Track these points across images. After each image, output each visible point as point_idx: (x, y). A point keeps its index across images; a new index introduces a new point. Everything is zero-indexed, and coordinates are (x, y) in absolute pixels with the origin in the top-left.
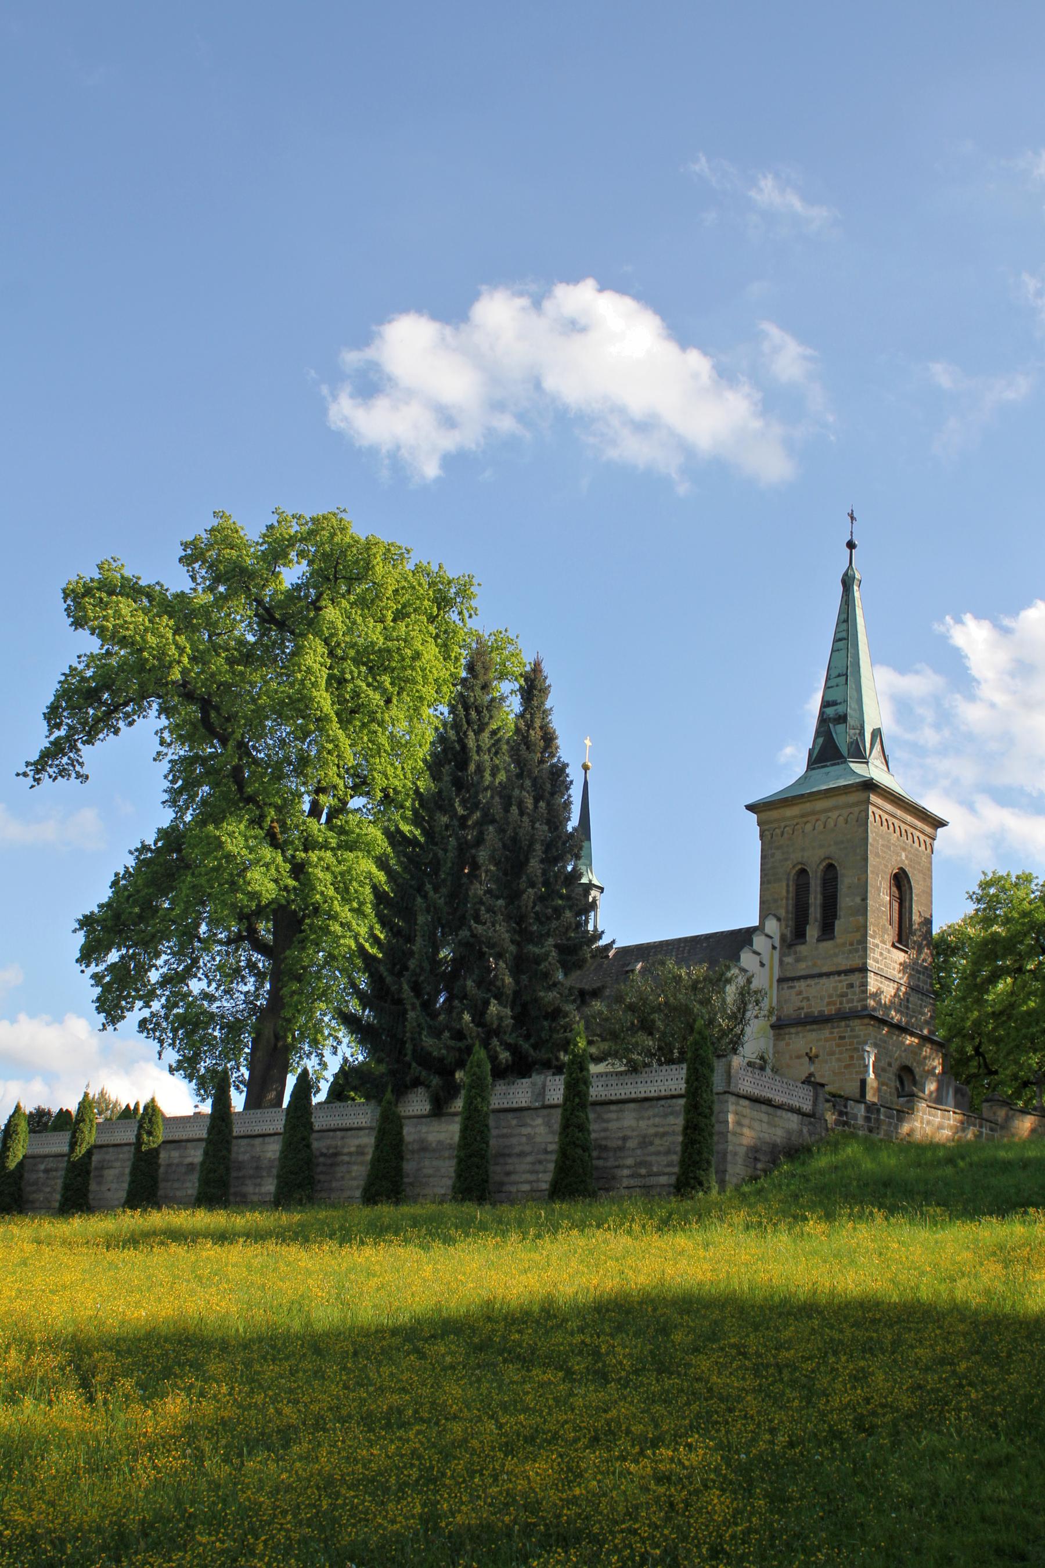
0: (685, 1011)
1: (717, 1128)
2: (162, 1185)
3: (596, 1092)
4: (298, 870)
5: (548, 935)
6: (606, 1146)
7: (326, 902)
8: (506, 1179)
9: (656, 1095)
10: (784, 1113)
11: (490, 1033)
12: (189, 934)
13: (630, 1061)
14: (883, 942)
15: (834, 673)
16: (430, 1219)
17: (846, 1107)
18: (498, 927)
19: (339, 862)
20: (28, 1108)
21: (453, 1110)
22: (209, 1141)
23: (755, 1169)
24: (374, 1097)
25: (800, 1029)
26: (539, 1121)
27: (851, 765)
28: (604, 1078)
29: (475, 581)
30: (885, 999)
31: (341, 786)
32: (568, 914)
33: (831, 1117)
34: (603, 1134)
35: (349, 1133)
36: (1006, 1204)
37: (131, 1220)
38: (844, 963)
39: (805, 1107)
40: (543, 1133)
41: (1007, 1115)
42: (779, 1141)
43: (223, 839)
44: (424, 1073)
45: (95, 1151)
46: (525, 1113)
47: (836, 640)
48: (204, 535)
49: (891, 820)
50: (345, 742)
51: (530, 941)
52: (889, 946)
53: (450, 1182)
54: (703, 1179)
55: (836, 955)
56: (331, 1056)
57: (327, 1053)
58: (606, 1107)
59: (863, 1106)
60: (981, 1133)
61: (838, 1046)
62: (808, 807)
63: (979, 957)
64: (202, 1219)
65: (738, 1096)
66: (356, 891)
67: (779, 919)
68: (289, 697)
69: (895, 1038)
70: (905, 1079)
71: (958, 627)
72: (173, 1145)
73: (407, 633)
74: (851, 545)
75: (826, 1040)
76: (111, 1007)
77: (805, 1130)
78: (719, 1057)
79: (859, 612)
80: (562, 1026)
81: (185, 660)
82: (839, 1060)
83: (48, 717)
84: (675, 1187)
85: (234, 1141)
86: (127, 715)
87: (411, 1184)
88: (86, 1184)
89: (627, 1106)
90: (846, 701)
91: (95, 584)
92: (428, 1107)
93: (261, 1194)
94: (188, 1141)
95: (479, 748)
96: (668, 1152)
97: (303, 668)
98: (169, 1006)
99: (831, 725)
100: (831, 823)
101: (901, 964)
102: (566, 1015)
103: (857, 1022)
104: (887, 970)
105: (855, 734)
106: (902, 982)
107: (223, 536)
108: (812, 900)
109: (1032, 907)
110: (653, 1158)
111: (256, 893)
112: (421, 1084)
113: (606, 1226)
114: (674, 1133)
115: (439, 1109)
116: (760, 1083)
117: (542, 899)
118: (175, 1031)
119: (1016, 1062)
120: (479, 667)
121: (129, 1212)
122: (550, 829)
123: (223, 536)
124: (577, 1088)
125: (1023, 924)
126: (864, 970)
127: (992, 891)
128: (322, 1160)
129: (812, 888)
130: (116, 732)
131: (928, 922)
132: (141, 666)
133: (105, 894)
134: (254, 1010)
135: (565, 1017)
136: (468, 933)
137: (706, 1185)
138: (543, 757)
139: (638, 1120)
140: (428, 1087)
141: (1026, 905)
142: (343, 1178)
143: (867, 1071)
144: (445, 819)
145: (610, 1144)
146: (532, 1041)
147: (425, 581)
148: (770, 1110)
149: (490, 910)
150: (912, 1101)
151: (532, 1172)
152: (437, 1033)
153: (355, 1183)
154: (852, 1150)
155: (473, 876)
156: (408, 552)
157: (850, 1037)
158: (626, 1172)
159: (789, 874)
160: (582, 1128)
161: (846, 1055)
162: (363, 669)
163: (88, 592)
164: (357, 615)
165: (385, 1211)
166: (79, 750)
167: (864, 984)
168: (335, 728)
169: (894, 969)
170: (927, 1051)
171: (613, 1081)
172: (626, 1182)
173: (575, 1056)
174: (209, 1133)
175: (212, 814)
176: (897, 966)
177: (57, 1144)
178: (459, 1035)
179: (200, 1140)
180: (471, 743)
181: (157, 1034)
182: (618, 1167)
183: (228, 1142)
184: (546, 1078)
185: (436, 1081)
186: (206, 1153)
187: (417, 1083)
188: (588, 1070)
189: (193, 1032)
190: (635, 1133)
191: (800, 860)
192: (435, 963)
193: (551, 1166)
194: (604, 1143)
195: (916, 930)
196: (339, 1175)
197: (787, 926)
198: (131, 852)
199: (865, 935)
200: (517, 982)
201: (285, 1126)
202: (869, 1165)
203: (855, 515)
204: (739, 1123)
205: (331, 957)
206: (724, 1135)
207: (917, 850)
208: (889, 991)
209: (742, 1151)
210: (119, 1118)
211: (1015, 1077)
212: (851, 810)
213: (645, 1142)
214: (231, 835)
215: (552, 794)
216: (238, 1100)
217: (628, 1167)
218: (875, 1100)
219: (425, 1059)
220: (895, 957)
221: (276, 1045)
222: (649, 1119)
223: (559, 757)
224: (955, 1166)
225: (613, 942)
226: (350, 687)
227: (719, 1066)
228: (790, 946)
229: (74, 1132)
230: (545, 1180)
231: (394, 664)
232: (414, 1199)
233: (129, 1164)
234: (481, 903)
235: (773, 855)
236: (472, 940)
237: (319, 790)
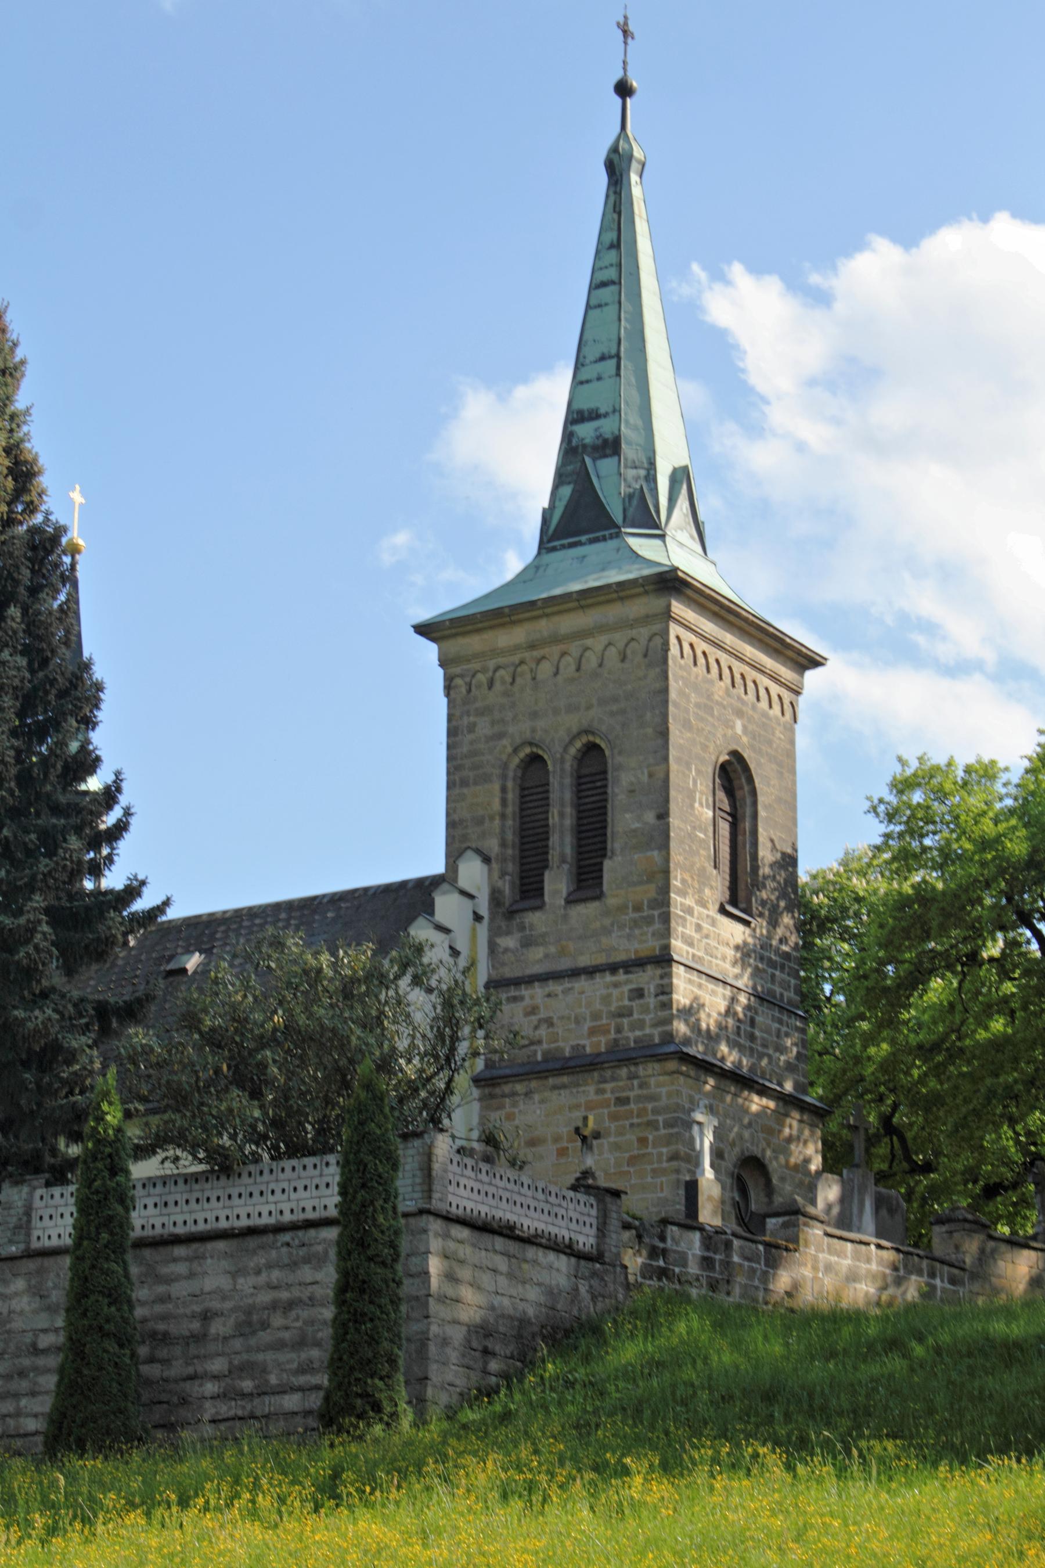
1: (408, 1287)
3: (145, 1218)
5: (31, 888)
6: (166, 1335)
9: (272, 1221)
10: (540, 1252)
14: (702, 903)
17: (663, 1239)
23: (485, 1372)
25: (534, 1084)
26: (20, 1284)
27: (633, 542)
28: (159, 1189)
30: (709, 1020)
32: (74, 843)
33: (634, 1261)
34: (159, 1309)
38: (625, 948)
39: (582, 1239)
41: (982, 1251)
42: (531, 1312)
47: (596, 285)
49: (714, 653)
52: (713, 911)
54: (382, 1396)
55: (607, 931)
59: (697, 1236)
60: (933, 1287)
61: (614, 1117)
62: (543, 627)
63: (892, 931)
65: (448, 1219)
67: (487, 860)
69: (729, 1098)
70: (750, 1184)
71: (718, 287)
74: (624, 90)
75: (590, 1107)
77: (583, 1290)
78: (405, 1137)
80: (64, 1082)
82: (617, 1147)
84: (321, 1416)
89: (210, 1246)
90: (616, 410)
96: (301, 1343)
99: (588, 460)
100: (591, 661)
101: (737, 948)
102: (71, 1057)
104: (710, 963)
105: (637, 479)
106: (740, 984)
108: (554, 818)
109: (1002, 827)
110: (269, 1357)
113: (201, 1501)
114: (312, 1301)
116: (491, 1190)
122: (30, 664)
125: (983, 864)
126: (664, 960)
127: (917, 797)
129: (554, 796)
131: (789, 861)
135: (69, 1063)
137: (388, 1409)
138: (11, 511)
139: (234, 1275)
141: (988, 827)
145: (174, 1329)
148: (512, 1247)
150: (796, 1225)
154: (686, 1327)
157: (639, 1099)
158: (210, 1388)
159: (505, 766)
160: (118, 1296)
161: (631, 1137)
167: (666, 990)
169: (724, 958)
170: (792, 1125)
171: (179, 1193)
172: (210, 1410)
173: (98, 1142)
176: (730, 953)
182: (191, 1378)
184: (31, 1194)
188: (127, 1172)
190: (228, 1305)
191: (528, 735)
193: (50, 1382)
194: (161, 1327)
195: (765, 877)
197: (503, 874)
199: (665, 889)
202: (726, 1358)
203: (632, 27)
204: (450, 1277)
206: (422, 1301)
207: (765, 715)
208: (714, 1004)
209: (457, 1335)
211: (972, 1175)
212: (634, 633)
213: (249, 1324)
215: (34, 591)
217: (215, 1377)
218: (717, 1222)
220: (725, 935)
222: (258, 1272)
223: (48, 513)
224: (906, 1355)
225: (167, 903)
227: (409, 1156)
228: (511, 914)
235: (472, 728)
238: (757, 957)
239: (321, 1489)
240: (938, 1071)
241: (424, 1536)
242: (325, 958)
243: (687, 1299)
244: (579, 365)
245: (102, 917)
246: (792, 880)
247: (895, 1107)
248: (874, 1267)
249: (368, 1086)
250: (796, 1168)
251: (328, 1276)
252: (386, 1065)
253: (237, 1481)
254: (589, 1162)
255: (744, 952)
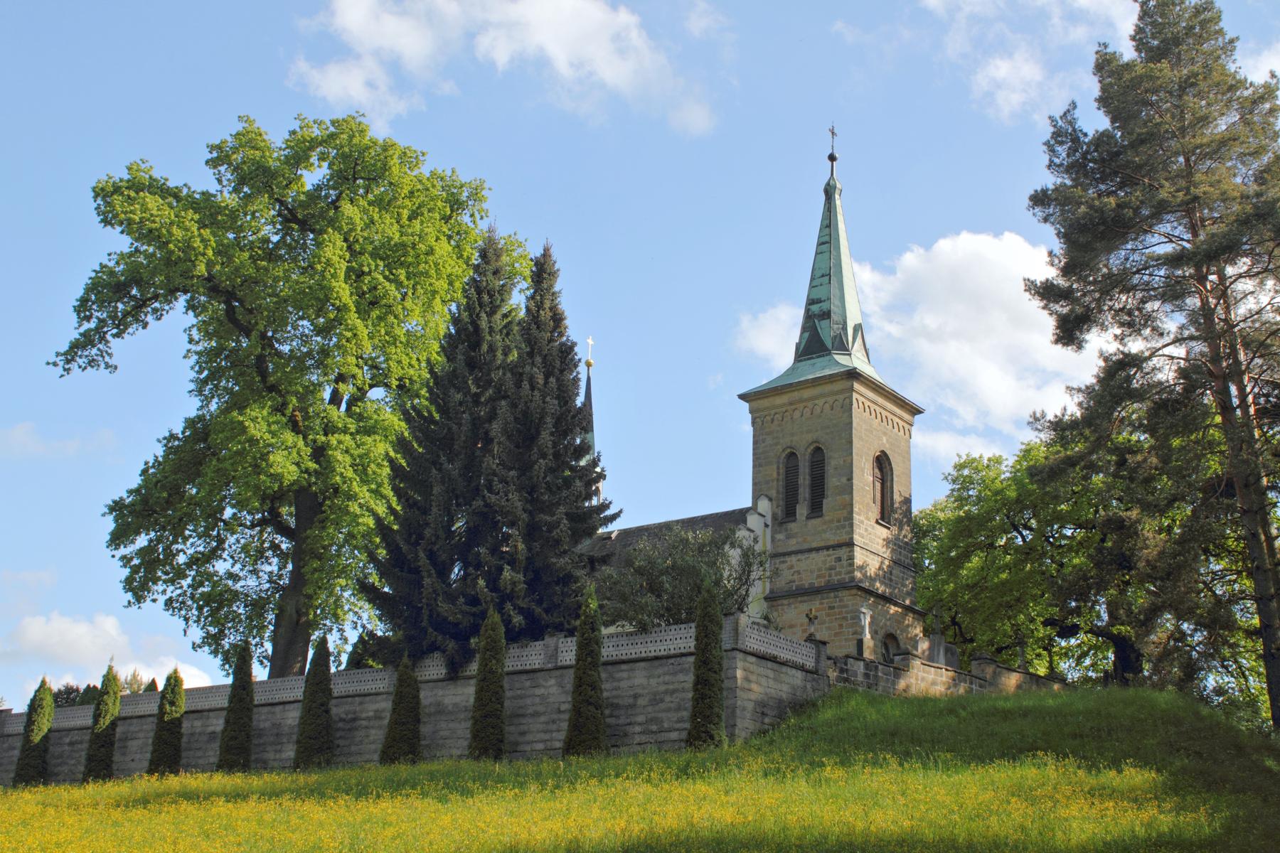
0: (692, 572)
1: (727, 684)
2: (184, 754)
3: (608, 651)
4: (319, 453)
7: (345, 482)
8: (521, 739)
11: (504, 597)
12: (213, 516)
13: (640, 622)
15: (818, 274)
16: (448, 774)
18: (510, 496)
19: (358, 446)
20: (56, 685)
21: (468, 673)
22: (229, 710)
24: (392, 662)
26: (553, 682)
29: (486, 185)
31: (360, 375)
33: (833, 674)
34: (615, 693)
35: (368, 699)
36: (1014, 750)
37: (148, 784)
38: (833, 539)
40: (556, 694)
42: (784, 696)
43: (247, 424)
44: (440, 638)
45: (119, 723)
46: (539, 674)
47: (820, 244)
48: (229, 139)
49: (873, 407)
50: (363, 332)
51: (542, 511)
52: (873, 522)
53: (466, 743)
54: (714, 732)
55: (825, 531)
56: (351, 625)
57: (347, 627)
58: (618, 667)
61: (828, 615)
62: (796, 395)
64: (219, 780)
65: (745, 652)
66: (374, 473)
67: (770, 500)
68: (310, 288)
72: (195, 715)
73: (422, 230)
74: (832, 158)
76: (138, 588)
78: (726, 615)
79: (840, 218)
81: (210, 252)
82: (829, 628)
83: (78, 310)
85: (255, 710)
86: (155, 310)
87: (428, 746)
88: (109, 756)
90: (829, 299)
91: (124, 184)
92: (444, 671)
93: (281, 760)
94: (210, 710)
95: (491, 330)
96: (678, 709)
97: (323, 260)
98: (195, 586)
100: (818, 409)
102: (576, 580)
103: (845, 593)
104: (871, 545)
107: (248, 139)
108: (801, 481)
110: (663, 715)
111: (278, 475)
112: (437, 649)
114: (684, 690)
115: (454, 673)
117: (551, 470)
118: (200, 609)
119: (993, 630)
120: (490, 254)
121: (146, 776)
123: (248, 139)
124: (588, 650)
125: (996, 501)
126: (850, 544)
127: (966, 472)
128: (341, 725)
129: (801, 470)
130: (145, 325)
131: (907, 501)
132: (168, 262)
133: (135, 481)
134: (278, 588)
136: (482, 503)
139: (648, 678)
140: (444, 652)
141: (998, 485)
142: (361, 742)
143: (862, 632)
144: (459, 396)
146: (544, 605)
147: (439, 184)
148: (775, 666)
149: (504, 481)
151: (545, 732)
152: (451, 598)
153: (373, 747)
154: (853, 704)
155: (487, 449)
156: (423, 154)
157: (840, 607)
158: (638, 729)
160: (594, 687)
161: (836, 624)
162: (381, 263)
163: (117, 190)
164: (375, 213)
165: (403, 770)
166: (107, 342)
167: (851, 558)
168: (353, 318)
170: (909, 619)
171: (624, 641)
172: (637, 739)
174: (230, 702)
175: (237, 402)
176: (881, 542)
177: (83, 717)
178: (474, 601)
179: (222, 709)
180: (484, 324)
181: (183, 612)
182: (630, 724)
183: (250, 710)
185: (451, 645)
186: (227, 722)
187: (434, 648)
189: (218, 609)
192: (450, 534)
193: (565, 725)
194: (615, 701)
196: (358, 739)
198: (159, 441)
199: (851, 512)
200: (530, 549)
201: (305, 692)
204: (747, 679)
205: (351, 536)
206: (733, 690)
208: (873, 565)
209: (750, 706)
210: (146, 690)
211: (991, 643)
213: (656, 700)
214: (254, 420)
215: (562, 371)
216: (260, 673)
218: (872, 658)
219: (441, 625)
221: (298, 621)
226: (367, 279)
227: (727, 624)
228: (781, 524)
229: (99, 704)
230: (559, 739)
231: (410, 260)
232: (433, 758)
233: (152, 734)
234: (495, 474)
236: (485, 510)
237: (341, 378)
238: (892, 543)
239: (681, 771)
240: (975, 597)
241: (727, 793)
242: (690, 535)
243: (857, 691)
244: (812, 279)
245: (591, 517)
246: (909, 510)
247: (956, 613)
248: (944, 679)
249: (708, 591)
250: (911, 639)
251: (690, 678)
252: (717, 583)
253: (643, 766)
254: (812, 630)
255: (888, 542)
